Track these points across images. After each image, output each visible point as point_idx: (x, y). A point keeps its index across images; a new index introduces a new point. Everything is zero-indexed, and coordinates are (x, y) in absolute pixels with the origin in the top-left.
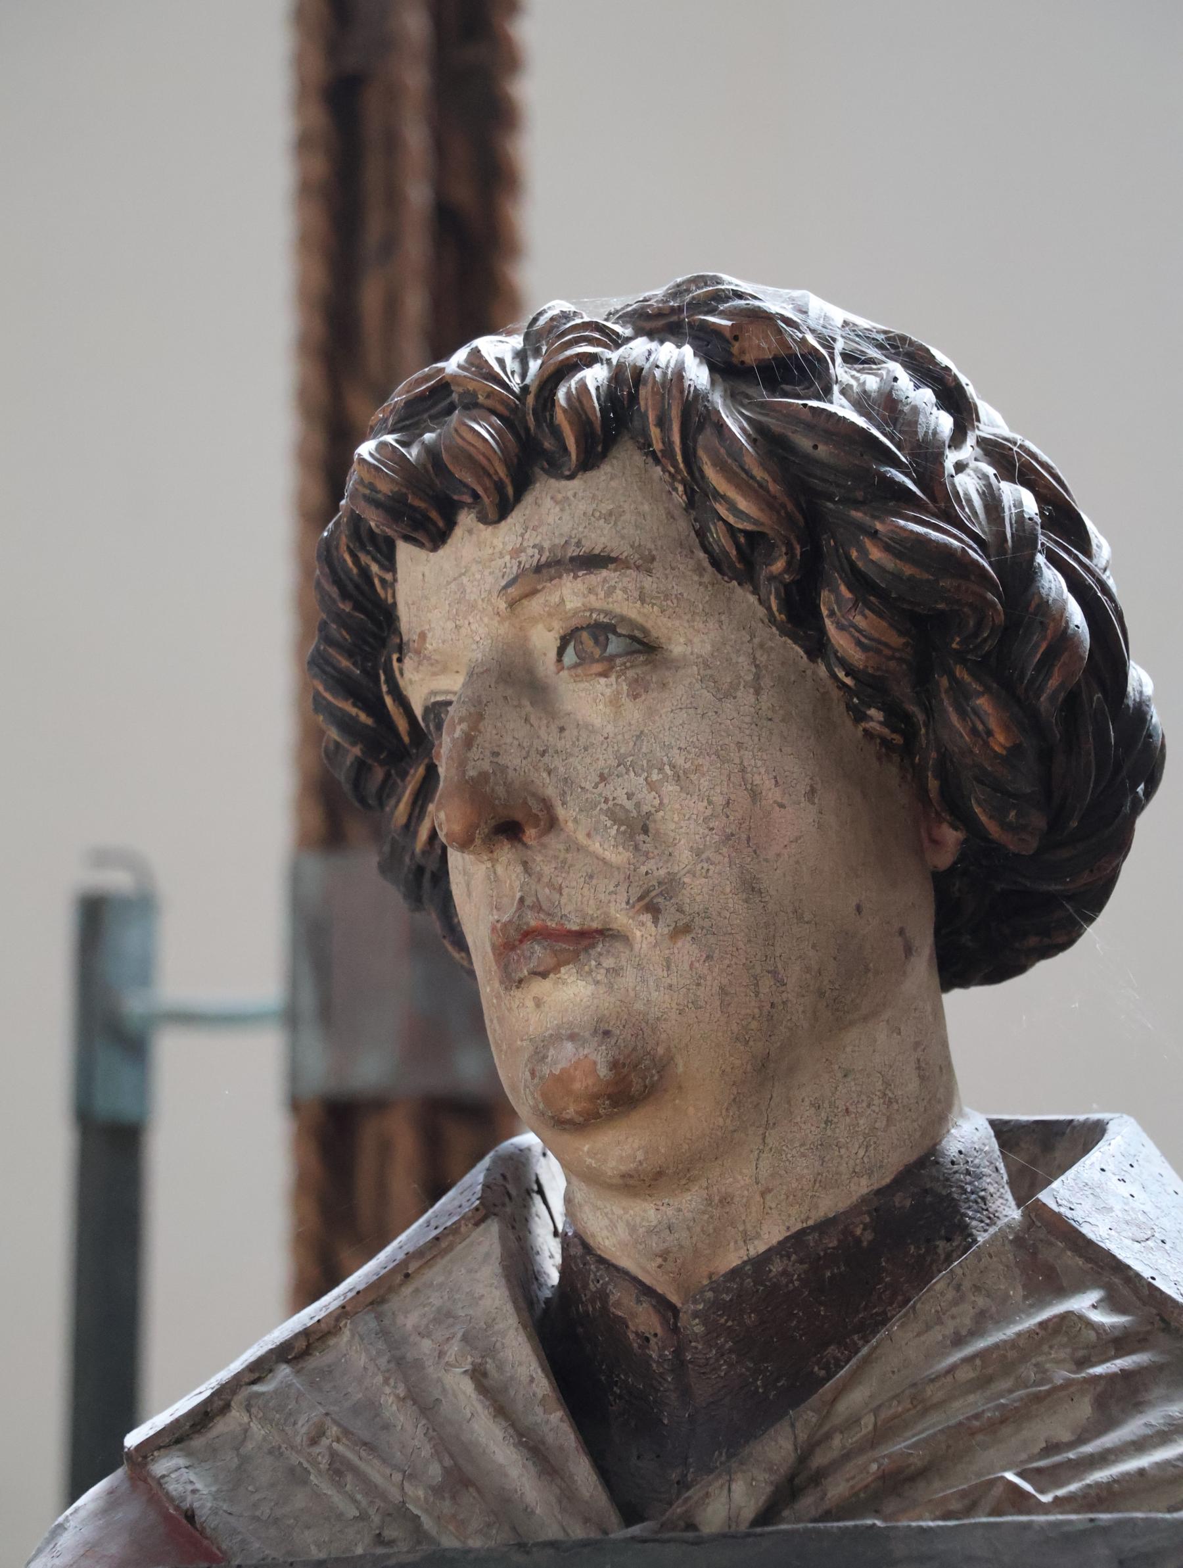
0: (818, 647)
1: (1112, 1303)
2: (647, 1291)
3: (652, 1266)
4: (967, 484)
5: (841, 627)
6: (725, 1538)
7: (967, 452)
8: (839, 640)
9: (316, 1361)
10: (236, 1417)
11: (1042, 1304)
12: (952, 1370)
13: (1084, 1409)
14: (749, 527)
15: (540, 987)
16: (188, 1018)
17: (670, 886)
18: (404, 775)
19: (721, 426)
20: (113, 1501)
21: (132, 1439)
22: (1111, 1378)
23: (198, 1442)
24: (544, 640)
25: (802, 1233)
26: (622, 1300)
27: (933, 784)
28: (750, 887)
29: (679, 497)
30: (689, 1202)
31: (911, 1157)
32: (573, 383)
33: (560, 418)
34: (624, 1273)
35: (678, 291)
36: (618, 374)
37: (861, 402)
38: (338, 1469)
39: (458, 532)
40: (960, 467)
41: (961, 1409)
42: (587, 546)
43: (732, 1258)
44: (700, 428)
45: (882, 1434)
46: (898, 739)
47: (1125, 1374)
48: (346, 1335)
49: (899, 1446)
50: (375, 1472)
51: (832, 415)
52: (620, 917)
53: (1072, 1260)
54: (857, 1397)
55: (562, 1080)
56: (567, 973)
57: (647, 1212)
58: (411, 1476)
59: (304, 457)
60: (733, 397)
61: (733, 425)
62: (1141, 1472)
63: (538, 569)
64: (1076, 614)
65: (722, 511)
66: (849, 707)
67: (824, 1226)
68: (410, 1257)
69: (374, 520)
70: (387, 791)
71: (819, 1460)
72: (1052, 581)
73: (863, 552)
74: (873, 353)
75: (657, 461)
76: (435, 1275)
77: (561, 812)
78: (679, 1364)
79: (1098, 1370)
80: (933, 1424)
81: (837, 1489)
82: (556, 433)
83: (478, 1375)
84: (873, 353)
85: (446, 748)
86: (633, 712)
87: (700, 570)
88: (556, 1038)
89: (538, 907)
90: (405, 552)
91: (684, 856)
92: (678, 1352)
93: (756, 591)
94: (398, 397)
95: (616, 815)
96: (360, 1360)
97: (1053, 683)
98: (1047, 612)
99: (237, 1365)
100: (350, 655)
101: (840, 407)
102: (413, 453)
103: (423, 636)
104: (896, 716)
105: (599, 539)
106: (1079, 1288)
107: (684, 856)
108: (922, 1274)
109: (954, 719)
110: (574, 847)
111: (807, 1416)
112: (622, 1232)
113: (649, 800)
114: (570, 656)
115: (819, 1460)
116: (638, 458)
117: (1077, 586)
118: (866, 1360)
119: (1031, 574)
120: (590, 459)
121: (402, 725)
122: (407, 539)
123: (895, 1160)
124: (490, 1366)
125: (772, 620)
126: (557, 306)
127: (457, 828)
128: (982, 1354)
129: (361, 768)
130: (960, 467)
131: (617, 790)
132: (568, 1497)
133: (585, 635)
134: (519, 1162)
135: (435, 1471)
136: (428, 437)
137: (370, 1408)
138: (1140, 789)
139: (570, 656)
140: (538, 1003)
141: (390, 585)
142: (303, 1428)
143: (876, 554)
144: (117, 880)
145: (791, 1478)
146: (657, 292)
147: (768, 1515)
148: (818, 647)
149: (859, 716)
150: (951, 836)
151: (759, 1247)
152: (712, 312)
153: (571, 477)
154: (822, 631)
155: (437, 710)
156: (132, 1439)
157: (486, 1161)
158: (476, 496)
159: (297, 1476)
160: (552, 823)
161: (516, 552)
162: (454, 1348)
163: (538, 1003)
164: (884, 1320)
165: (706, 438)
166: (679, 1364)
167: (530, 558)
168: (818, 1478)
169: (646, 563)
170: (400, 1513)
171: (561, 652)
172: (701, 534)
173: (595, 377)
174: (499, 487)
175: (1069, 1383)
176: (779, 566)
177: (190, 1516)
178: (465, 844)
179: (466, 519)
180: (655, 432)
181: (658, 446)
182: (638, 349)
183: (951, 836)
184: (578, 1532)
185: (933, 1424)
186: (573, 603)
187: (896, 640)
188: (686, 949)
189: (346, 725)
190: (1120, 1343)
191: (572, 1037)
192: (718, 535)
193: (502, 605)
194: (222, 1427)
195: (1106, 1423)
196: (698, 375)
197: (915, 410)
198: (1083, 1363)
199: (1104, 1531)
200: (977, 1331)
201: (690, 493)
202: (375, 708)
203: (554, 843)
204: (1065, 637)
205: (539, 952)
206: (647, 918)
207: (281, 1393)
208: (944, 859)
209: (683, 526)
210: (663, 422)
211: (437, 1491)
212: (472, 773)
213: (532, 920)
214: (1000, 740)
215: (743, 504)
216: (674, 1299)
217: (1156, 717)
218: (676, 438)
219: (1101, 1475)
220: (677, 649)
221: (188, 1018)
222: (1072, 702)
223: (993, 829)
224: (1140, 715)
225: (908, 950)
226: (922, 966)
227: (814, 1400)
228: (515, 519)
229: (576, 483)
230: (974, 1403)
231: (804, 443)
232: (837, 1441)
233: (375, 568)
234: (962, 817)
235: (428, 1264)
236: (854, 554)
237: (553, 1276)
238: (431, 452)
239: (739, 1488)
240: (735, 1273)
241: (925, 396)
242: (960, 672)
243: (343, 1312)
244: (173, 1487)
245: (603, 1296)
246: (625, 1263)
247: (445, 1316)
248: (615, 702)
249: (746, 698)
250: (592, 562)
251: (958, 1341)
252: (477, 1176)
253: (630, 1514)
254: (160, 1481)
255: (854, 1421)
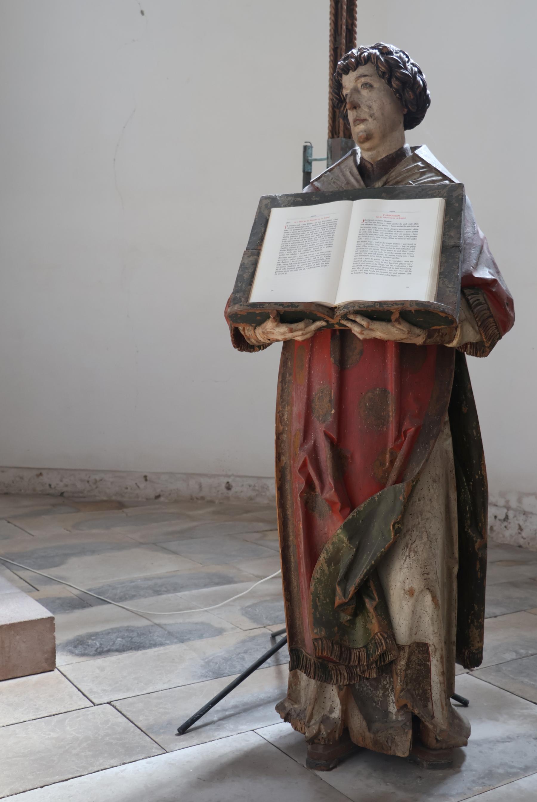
0: (391, 86)
1: (422, 163)
2: (370, 163)
3: (370, 159)
4: (409, 67)
5: (394, 83)
6: (378, 188)
7: (409, 63)
8: (394, 85)
9: (332, 172)
10: (323, 178)
11: (414, 164)
12: (404, 170)
13: (419, 175)
14: (383, 71)
15: (358, 126)
16: (316, 160)
17: (374, 114)
18: (343, 104)
19: (381, 59)
20: (309, 187)
21: (311, 181)
22: (422, 172)
23: (319, 181)
24: (359, 85)
25: (387, 156)
26: (367, 164)
27: (404, 103)
28: (383, 114)
29: (376, 68)
30: (374, 152)
31: (400, 147)
32: (363, 54)
33: (362, 59)
34: (367, 161)
35: (376, 44)
36: (369, 53)
37: (397, 57)
38: (334, 182)
39: (350, 73)
40: (408, 65)
41: (405, 175)
42: (364, 74)
43: (379, 159)
44: (378, 59)
45: (395, 178)
46: (400, 98)
47: (423, 171)
48: (335, 169)
49: (398, 179)
50: (338, 183)
51: (394, 58)
52: (368, 118)
53: (418, 159)
54: (393, 174)
55: (361, 137)
56: (361, 124)
57: (370, 153)
58: (342, 183)
59: (330, 67)
60: (382, 56)
61: (382, 59)
62: (425, 182)
63: (359, 77)
64: (421, 83)
65: (380, 69)
66: (395, 94)
67: (390, 155)
68: (343, 160)
69: (340, 72)
70: (341, 107)
71: (388, 181)
72: (419, 79)
73: (397, 74)
74: (399, 52)
75: (373, 64)
76: (345, 162)
77: (361, 106)
78: (373, 170)
79: (421, 171)
80: (402, 176)
81: (391, 183)
82: (361, 60)
83: (350, 172)
84: (399, 52)
85: (348, 101)
86: (370, 94)
87: (378, 77)
88: (360, 132)
89: (358, 116)
90: (344, 76)
91: (375, 111)
92: (373, 169)
93: (384, 80)
94: (343, 57)
95: (367, 106)
96: (337, 171)
97: (418, 90)
98: (419, 82)
99: (323, 172)
100: (337, 89)
101: (394, 57)
102: (345, 63)
103: (345, 86)
104: (400, 95)
105: (366, 73)
106: (418, 162)
107: (375, 111)
108: (401, 161)
109: (407, 94)
110: (362, 110)
111: (387, 176)
112: (367, 156)
113: (371, 104)
114: (362, 87)
115: (388, 181)
116: (371, 64)
117: (421, 79)
118: (394, 170)
119: (416, 78)
120: (366, 63)
121: (343, 98)
122: (344, 74)
123: (398, 147)
124: (352, 171)
125: (386, 83)
126: (362, 46)
127: (349, 107)
128: (407, 169)
129: (338, 104)
130: (408, 65)
131: (368, 103)
132: (360, 185)
133: (364, 85)
134: (355, 151)
135: (345, 182)
136: (346, 62)
137: (338, 176)
138: (428, 105)
139: (362, 87)
140: (358, 128)
141: (341, 80)
142: (330, 178)
143: (398, 74)
144: (308, 144)
145: (385, 182)
146: (373, 45)
147: (383, 186)
148: (391, 86)
149: (396, 95)
150: (406, 110)
151: (382, 157)
152: (380, 46)
153: (363, 66)
154: (392, 84)
155: (347, 95)
156: (311, 181)
157: (351, 150)
158: (352, 68)
159: (330, 184)
160: (360, 107)
161: (356, 75)
162: (348, 170)
163: (358, 128)
164: (396, 165)
165: (379, 61)
166: (373, 170)
167: (358, 75)
168: (388, 182)
169: (371, 76)
170: (341, 187)
171: (361, 87)
172: (378, 73)
173: (366, 54)
174: (354, 67)
175: (417, 172)
176: (387, 76)
177: (318, 188)
178: (350, 109)
179: (351, 71)
180: (373, 60)
181: (373, 62)
182: (371, 51)
183: (406, 110)
184: (361, 188)
185: (402, 176)
186: (363, 81)
187: (400, 85)
188: (375, 121)
189: (336, 98)
190: (423, 168)
191: (362, 132)
192: (380, 73)
193: (355, 81)
194: (321, 179)
195: (421, 176)
196: (378, 53)
197: (403, 58)
198: (419, 170)
199: (420, 186)
200: (407, 166)
201: (377, 68)
202: (340, 96)
203: (360, 109)
204: (420, 85)
205: (358, 122)
206: (371, 118)
207: (328, 175)
208: (405, 112)
209: (376, 72)
210: (374, 59)
211: (345, 184)
212: (351, 101)
213: (357, 118)
214: (412, 97)
215: (383, 68)
216: (373, 163)
217: (430, 96)
218: (375, 61)
219: (420, 182)
220: (375, 86)
221: (316, 160)
222: (420, 93)
223: (411, 108)
224: (428, 96)
225: (401, 123)
226: (402, 126)
227: (388, 174)
228: (356, 71)
229: (364, 67)
230: (407, 174)
231: (390, 61)
232: (391, 178)
233: (340, 78)
234: (407, 106)
235: (344, 161)
236: (396, 74)
237: (359, 163)
238: (347, 63)
239: (380, 183)
240: (380, 160)
241: (405, 56)
242: (408, 89)
243: (335, 166)
244: (316, 185)
245: (364, 163)
246: (367, 159)
247: (346, 166)
248: (367, 93)
249: (383, 92)
250: (365, 76)
251: (405, 168)
252: (350, 152)
253: (367, 187)
254: (314, 185)
255: (393, 176)
